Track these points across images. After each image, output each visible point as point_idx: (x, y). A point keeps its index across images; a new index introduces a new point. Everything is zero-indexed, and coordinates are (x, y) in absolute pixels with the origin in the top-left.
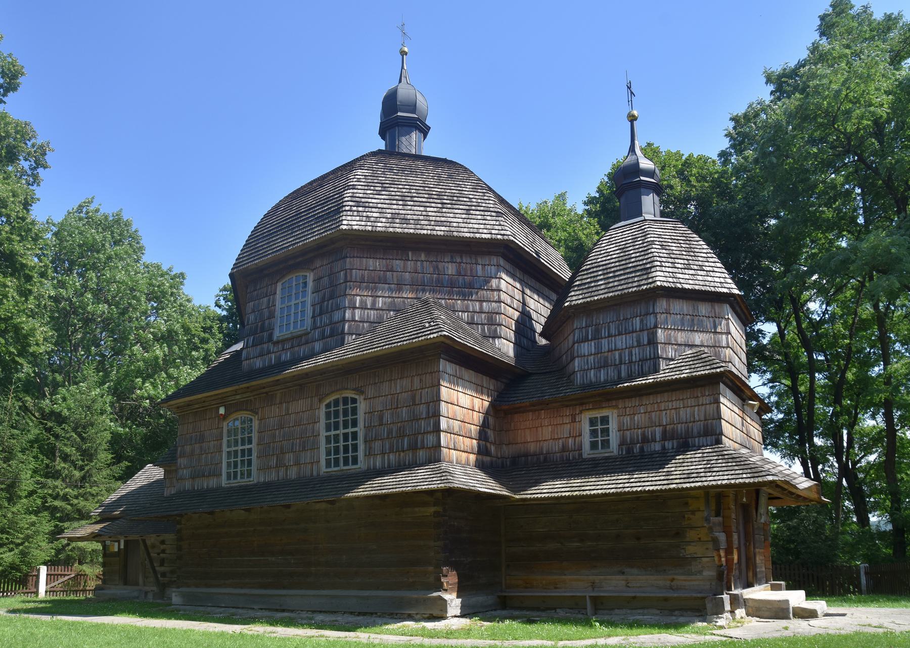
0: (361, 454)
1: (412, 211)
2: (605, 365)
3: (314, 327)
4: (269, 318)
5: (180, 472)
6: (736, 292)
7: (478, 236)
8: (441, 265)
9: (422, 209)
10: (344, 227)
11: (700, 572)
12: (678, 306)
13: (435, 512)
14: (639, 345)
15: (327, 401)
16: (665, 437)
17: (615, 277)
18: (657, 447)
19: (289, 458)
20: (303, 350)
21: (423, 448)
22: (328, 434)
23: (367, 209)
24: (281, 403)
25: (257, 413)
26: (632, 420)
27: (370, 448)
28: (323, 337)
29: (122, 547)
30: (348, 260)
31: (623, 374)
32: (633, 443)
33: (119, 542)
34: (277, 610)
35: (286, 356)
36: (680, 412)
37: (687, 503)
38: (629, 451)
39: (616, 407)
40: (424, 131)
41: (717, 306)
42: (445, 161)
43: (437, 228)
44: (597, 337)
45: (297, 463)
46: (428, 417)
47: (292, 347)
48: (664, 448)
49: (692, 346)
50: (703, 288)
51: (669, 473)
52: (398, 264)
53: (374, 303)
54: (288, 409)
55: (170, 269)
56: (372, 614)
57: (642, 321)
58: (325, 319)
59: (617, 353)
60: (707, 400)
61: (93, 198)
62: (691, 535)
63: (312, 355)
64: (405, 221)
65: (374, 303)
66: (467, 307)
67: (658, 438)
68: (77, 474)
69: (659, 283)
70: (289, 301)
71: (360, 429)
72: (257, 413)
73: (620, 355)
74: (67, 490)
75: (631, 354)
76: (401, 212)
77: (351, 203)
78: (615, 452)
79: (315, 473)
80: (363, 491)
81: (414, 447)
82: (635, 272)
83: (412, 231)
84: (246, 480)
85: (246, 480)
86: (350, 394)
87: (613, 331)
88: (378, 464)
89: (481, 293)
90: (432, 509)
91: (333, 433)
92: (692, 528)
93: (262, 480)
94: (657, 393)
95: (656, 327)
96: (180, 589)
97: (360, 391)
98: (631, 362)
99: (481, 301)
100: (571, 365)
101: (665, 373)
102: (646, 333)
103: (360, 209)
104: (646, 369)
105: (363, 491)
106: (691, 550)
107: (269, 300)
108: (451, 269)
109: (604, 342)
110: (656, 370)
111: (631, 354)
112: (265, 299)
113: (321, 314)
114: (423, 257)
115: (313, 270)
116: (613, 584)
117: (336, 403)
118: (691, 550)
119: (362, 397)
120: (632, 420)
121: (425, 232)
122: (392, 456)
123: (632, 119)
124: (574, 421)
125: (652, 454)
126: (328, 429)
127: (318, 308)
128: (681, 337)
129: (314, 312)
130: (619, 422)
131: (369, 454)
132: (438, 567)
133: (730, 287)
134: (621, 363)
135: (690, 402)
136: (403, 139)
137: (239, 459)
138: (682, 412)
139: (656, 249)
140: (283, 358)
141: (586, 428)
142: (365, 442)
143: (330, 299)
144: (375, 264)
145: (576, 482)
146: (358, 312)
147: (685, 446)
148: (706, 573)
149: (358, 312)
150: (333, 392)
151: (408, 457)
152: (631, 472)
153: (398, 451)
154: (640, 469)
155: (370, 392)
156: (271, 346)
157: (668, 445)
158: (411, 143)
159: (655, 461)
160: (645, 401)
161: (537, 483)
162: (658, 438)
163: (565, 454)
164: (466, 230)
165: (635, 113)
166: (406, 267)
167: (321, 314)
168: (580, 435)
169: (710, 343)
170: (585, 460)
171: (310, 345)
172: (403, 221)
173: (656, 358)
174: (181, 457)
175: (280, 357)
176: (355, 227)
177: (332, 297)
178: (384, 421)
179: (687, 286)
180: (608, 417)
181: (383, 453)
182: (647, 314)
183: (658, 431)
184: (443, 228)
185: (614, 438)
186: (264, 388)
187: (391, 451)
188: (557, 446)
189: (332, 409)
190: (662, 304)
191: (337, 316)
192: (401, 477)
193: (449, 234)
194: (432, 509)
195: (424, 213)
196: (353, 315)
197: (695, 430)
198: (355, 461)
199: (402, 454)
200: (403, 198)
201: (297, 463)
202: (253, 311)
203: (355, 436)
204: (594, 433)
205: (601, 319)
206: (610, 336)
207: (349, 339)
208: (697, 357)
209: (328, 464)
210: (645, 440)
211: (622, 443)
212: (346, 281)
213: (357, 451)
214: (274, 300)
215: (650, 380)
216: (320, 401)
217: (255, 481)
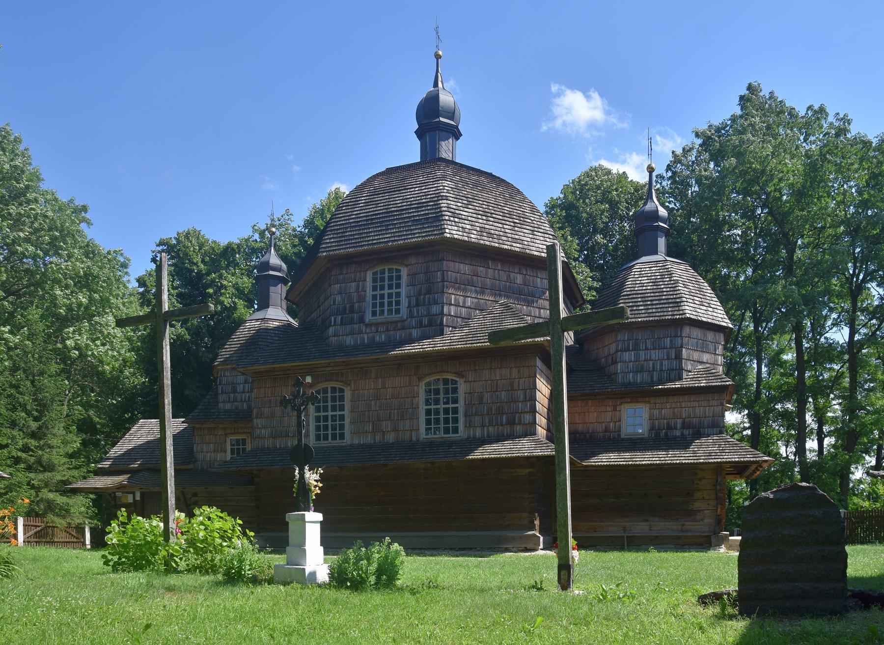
0: (461, 425)
1: (493, 227)
2: (641, 370)
3: (411, 316)
5: (258, 432)
6: (731, 326)
8: (512, 275)
9: (500, 225)
10: (448, 235)
11: (702, 520)
12: (696, 333)
13: (529, 473)
14: (668, 359)
16: (684, 426)
17: (652, 305)
18: (678, 433)
19: (386, 425)
20: (399, 335)
21: (520, 423)
23: (461, 221)
24: (376, 378)
25: (349, 385)
26: (660, 412)
27: (470, 421)
28: (420, 325)
29: (138, 498)
30: (445, 262)
31: (655, 379)
32: (660, 429)
33: (134, 493)
35: (381, 338)
36: (699, 409)
37: (696, 474)
38: (657, 434)
39: (649, 402)
40: (456, 134)
41: (717, 334)
42: (489, 175)
43: (514, 245)
44: (636, 348)
45: (395, 429)
46: (525, 400)
47: (387, 330)
48: (682, 434)
49: (702, 363)
50: (714, 322)
51: (694, 452)
52: (481, 270)
53: (464, 302)
55: (71, 201)
56: (471, 549)
57: (671, 341)
58: (422, 310)
59: (651, 363)
60: (715, 403)
62: (698, 495)
63: (411, 341)
64: (490, 235)
65: (464, 302)
66: (530, 312)
67: (679, 426)
68: (34, 425)
69: (688, 315)
71: (461, 406)
73: (653, 364)
74: (26, 440)
75: (661, 365)
76: (487, 226)
79: (414, 439)
80: (479, 454)
81: (511, 423)
82: (669, 303)
83: (497, 245)
84: (338, 441)
86: (450, 377)
87: (649, 346)
89: (540, 301)
90: (527, 471)
92: (699, 490)
93: (356, 441)
94: (680, 395)
95: (682, 347)
96: (262, 534)
97: (461, 375)
98: (661, 370)
99: (540, 308)
101: (686, 382)
102: (674, 350)
103: (456, 220)
104: (672, 376)
105: (479, 454)
106: (698, 505)
107: (358, 286)
108: (519, 279)
109: (642, 353)
110: (680, 378)
111: (661, 365)
112: (353, 284)
113: (418, 305)
114: (499, 267)
115: (407, 266)
116: (640, 528)
118: (698, 505)
120: (660, 412)
121: (506, 247)
122: (491, 429)
123: (438, 57)
125: (675, 438)
126: (427, 402)
128: (696, 356)
129: (409, 303)
130: (650, 414)
131: (469, 425)
132: (532, 513)
133: (726, 323)
134: (653, 370)
135: (704, 403)
136: (443, 143)
138: (697, 410)
139: (680, 286)
140: (377, 338)
142: (466, 415)
143: (428, 295)
144: (465, 268)
145: (627, 455)
147: (698, 434)
148: (706, 521)
149: (453, 308)
150: (432, 373)
151: (507, 430)
152: (667, 450)
153: (497, 424)
154: (673, 448)
155: (471, 376)
156: (363, 328)
157: (686, 432)
158: (446, 149)
159: (683, 444)
160: (671, 399)
161: (594, 454)
162: (679, 426)
164: (534, 249)
165: (440, 53)
166: (488, 273)
167: (418, 305)
169: (712, 361)
170: (623, 439)
171: (407, 331)
173: (681, 369)
174: (257, 418)
175: (374, 337)
177: (429, 292)
178: (485, 400)
179: (704, 319)
181: (483, 426)
182: (676, 336)
183: (679, 421)
187: (491, 424)
188: (600, 428)
190: (687, 330)
191: (435, 309)
192: (508, 444)
193: (523, 251)
194: (527, 471)
196: (449, 311)
197: (706, 423)
199: (501, 428)
200: (485, 213)
201: (395, 429)
202: (340, 293)
203: (455, 411)
205: (640, 335)
206: (646, 349)
207: (447, 330)
208: (707, 371)
210: (669, 427)
212: (443, 281)
213: (344, 420)
214: (364, 287)
215: (678, 385)
216: (420, 379)
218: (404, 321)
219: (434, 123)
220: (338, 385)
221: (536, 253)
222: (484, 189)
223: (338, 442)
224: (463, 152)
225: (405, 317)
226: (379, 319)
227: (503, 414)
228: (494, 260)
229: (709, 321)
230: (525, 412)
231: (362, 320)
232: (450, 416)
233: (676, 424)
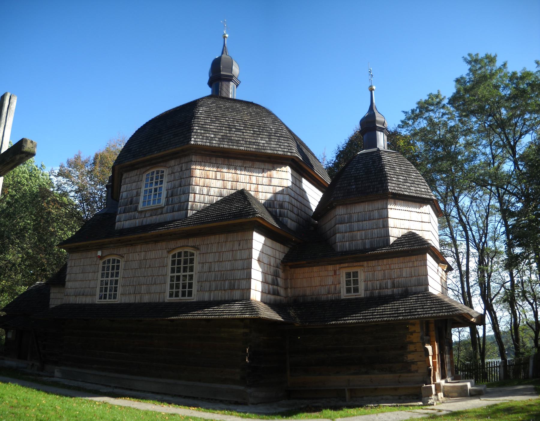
3: (167, 204)
4: (137, 196)
7: (275, 152)
10: (192, 142)
15: (174, 253)
16: (394, 286)
21: (238, 289)
22: (173, 275)
34: (127, 389)
54: (145, 215)
61: (403, 112)
64: (230, 140)
65: (208, 191)
70: (151, 186)
72: (123, 257)
77: (197, 128)
78: (363, 296)
81: (232, 288)
84: (352, 294)
85: (186, 298)
88: (206, 298)
90: (242, 331)
91: (176, 274)
93: (123, 301)
97: (197, 248)
100: (333, 238)
106: (410, 357)
117: (180, 254)
119: (198, 252)
124: (335, 273)
126: (173, 271)
127: (170, 192)
131: (200, 290)
137: (110, 271)
141: (343, 279)
146: (197, 196)
151: (226, 296)
156: (137, 214)
160: (380, 262)
162: (389, 285)
163: (329, 296)
168: (339, 283)
172: (230, 141)
176: (199, 143)
180: (357, 272)
184: (254, 146)
185: (362, 286)
186: (130, 241)
189: (176, 259)
191: (183, 198)
194: (242, 331)
195: (242, 136)
198: (190, 294)
204: (348, 283)
209: (171, 295)
211: (366, 290)
213: (346, 281)
217: (119, 302)
218: (162, 208)
219: (219, 75)
220: (116, 258)
221: (269, 151)
222: (238, 112)
223: (112, 301)
224: (233, 91)
225: (163, 205)
226: (147, 207)
227: (226, 280)
228: (217, 157)
229: (419, 195)
230: (243, 279)
231: (136, 209)
232: (352, 279)
233: (386, 284)
